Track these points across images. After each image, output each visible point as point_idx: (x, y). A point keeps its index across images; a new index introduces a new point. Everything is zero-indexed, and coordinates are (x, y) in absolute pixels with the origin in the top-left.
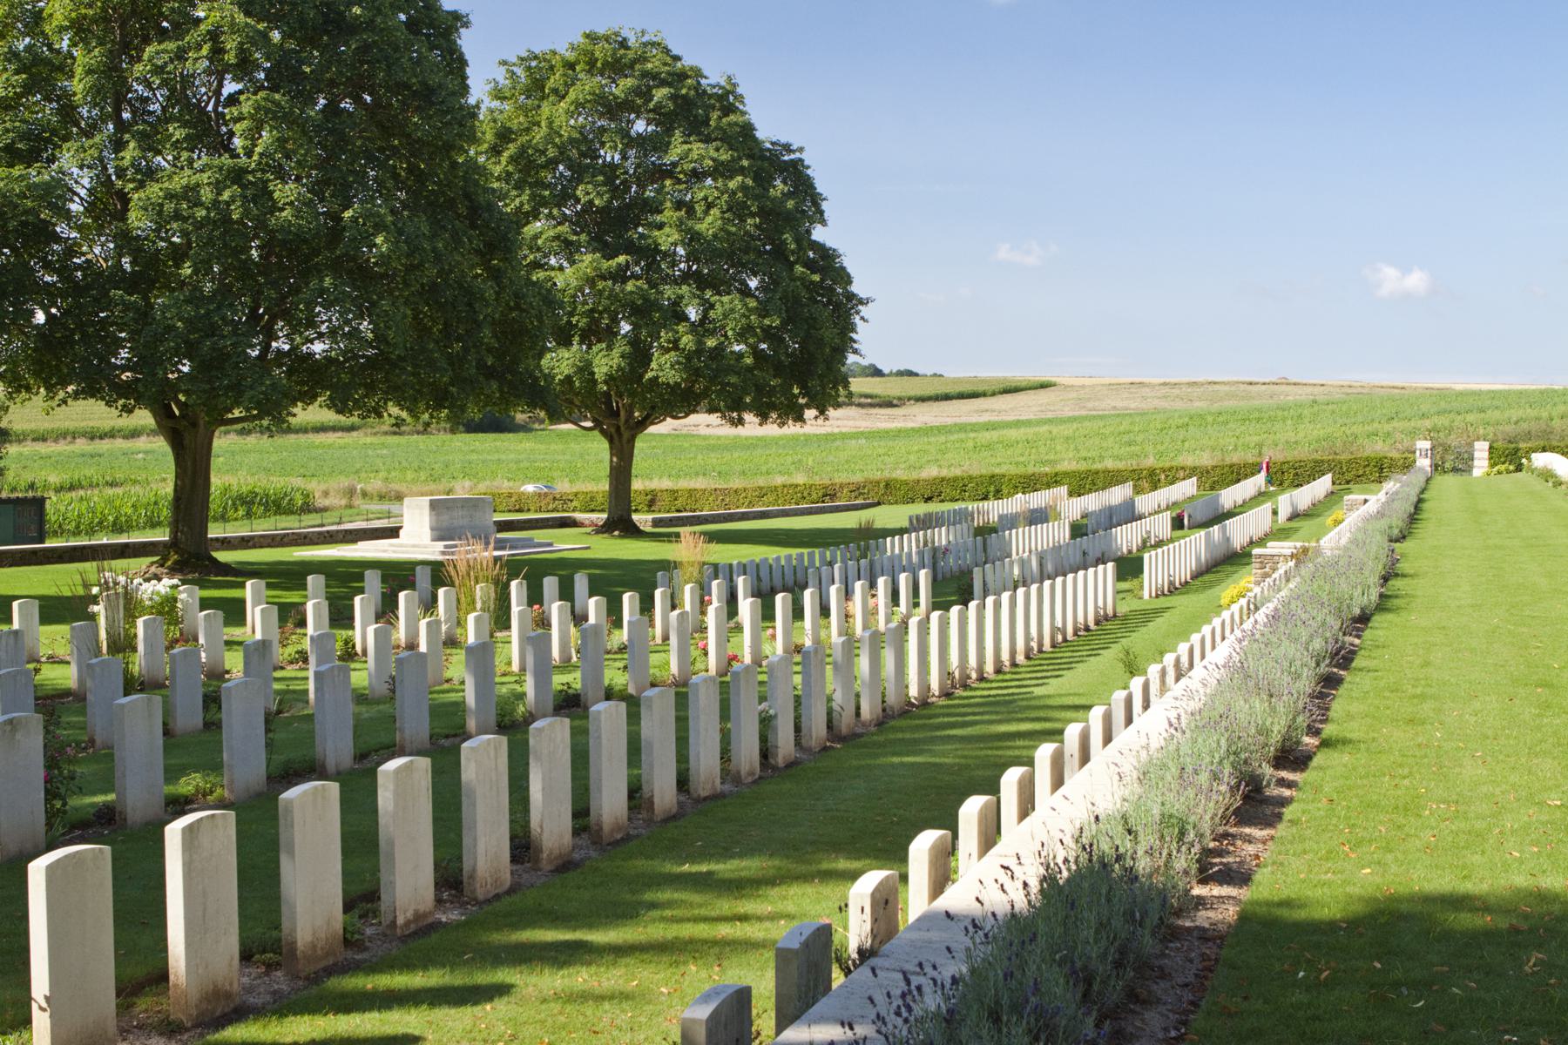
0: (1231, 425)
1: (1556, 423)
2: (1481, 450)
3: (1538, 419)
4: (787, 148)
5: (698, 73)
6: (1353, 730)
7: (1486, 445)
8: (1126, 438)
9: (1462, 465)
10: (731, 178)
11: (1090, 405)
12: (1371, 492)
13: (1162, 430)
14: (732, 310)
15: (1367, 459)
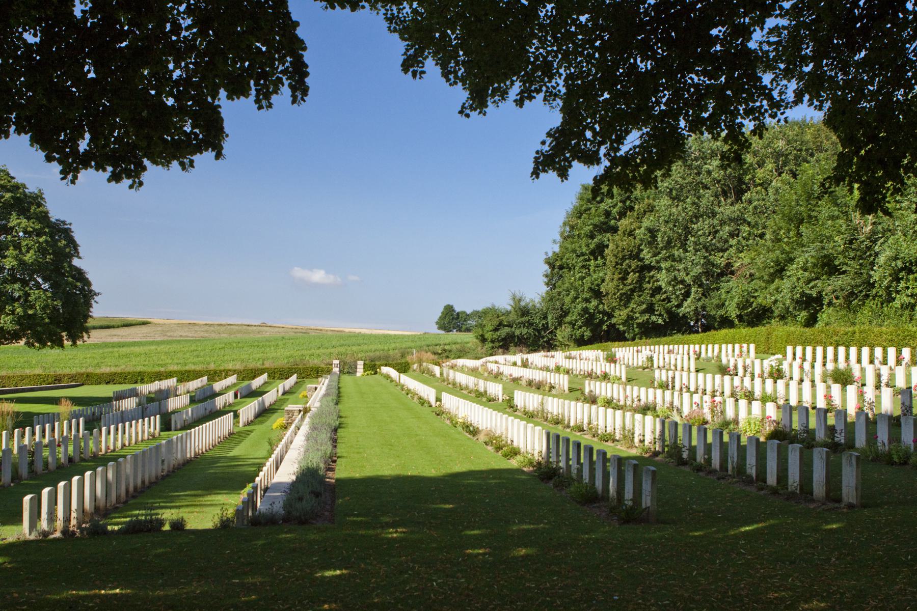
0: (245, 349)
2: (360, 364)
3: (383, 350)
4: (64, 223)
5: (24, 186)
7: (362, 362)
8: (195, 353)
9: (352, 371)
10: (41, 237)
11: (169, 334)
14: (40, 297)
15: (312, 368)
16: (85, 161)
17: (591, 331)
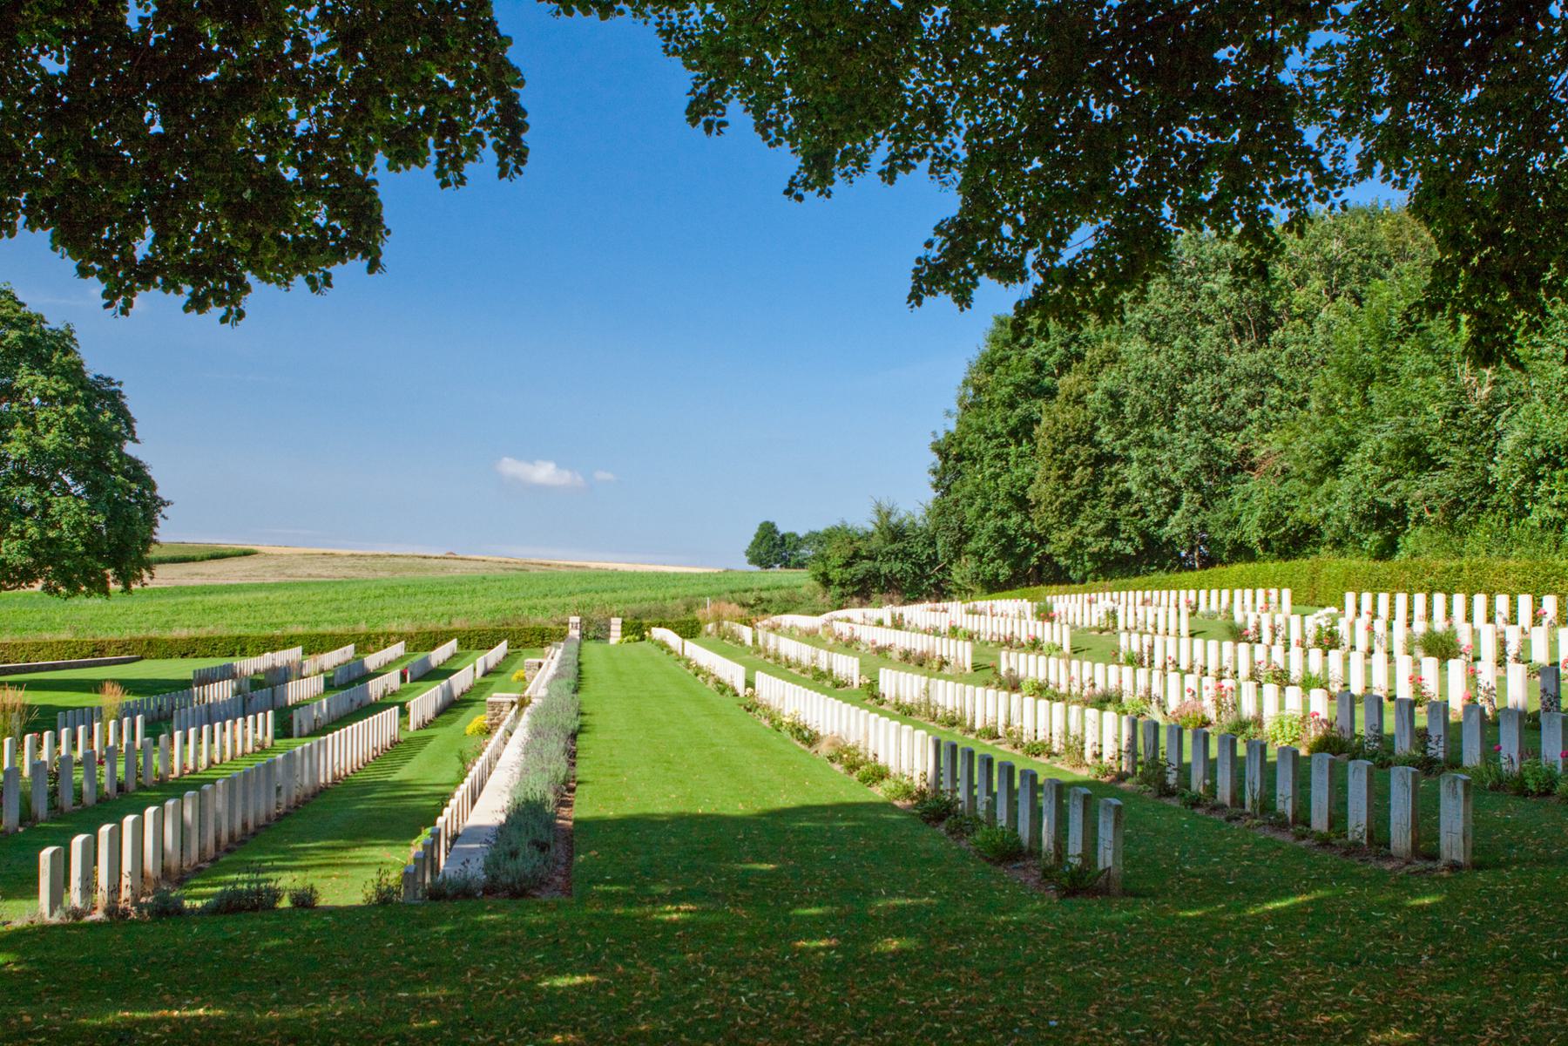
0: (419, 597)
1: (669, 603)
2: (616, 624)
3: (655, 599)
4: (109, 381)
5: (42, 319)
6: (588, 778)
7: (619, 621)
8: (334, 605)
9: (602, 634)
11: (288, 572)
12: (544, 656)
13: (362, 599)
14: (68, 509)
15: (533, 629)
16: (145, 274)
17: (1011, 566)
